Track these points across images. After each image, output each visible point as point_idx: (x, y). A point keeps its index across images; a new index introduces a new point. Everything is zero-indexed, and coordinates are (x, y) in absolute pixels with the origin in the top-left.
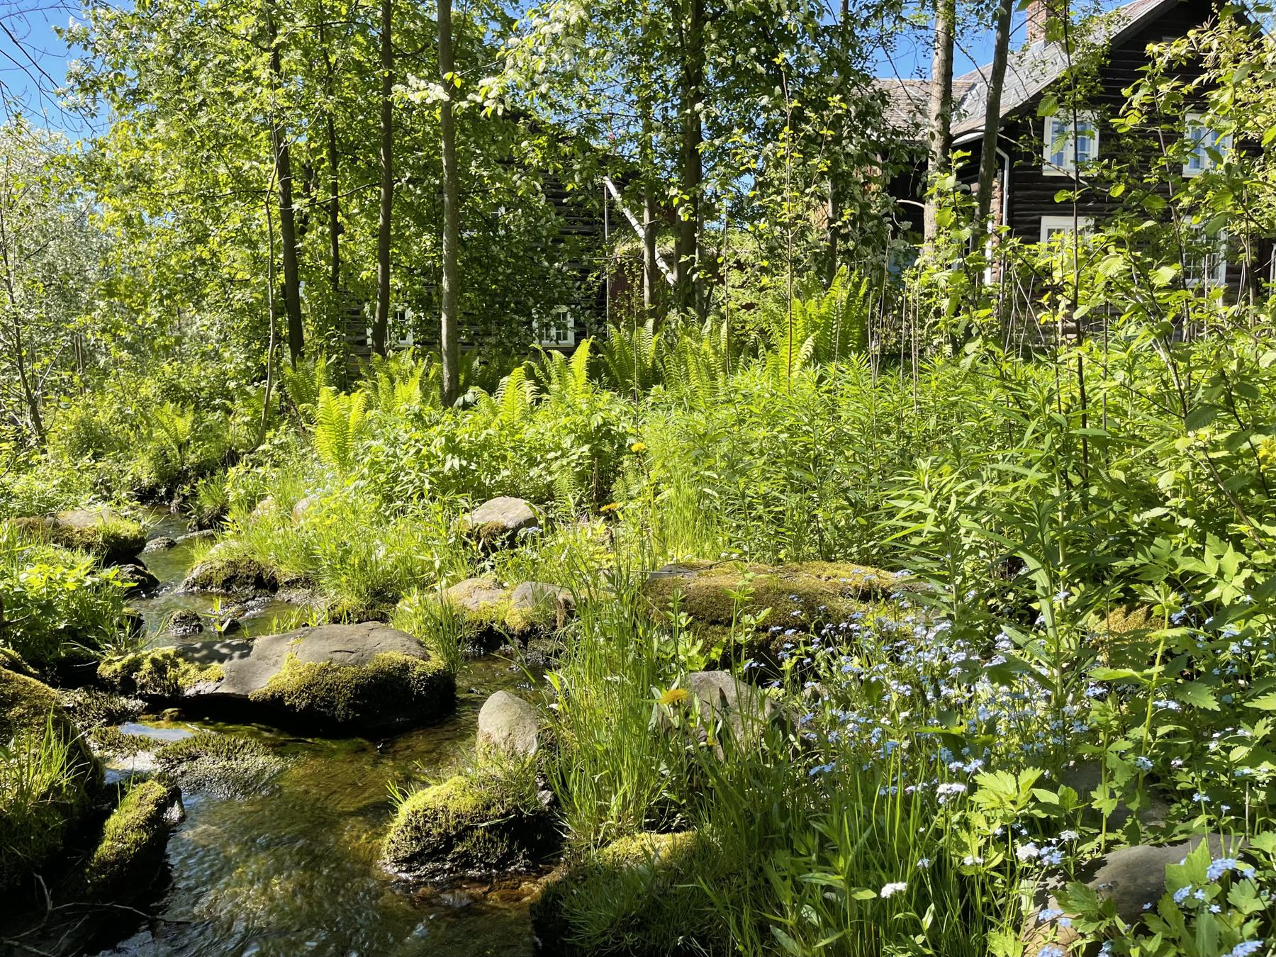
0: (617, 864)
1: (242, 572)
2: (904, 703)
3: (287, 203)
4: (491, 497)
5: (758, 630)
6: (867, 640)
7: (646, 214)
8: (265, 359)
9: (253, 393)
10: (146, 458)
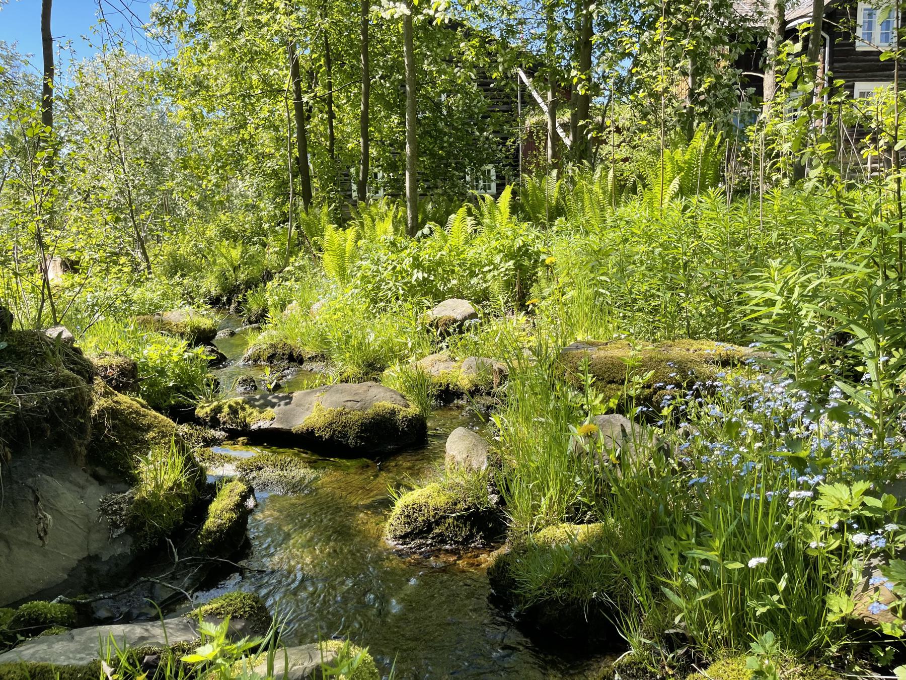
3: (299, 98)
4: (444, 299)
5: (643, 387)
6: (726, 393)
7: (549, 94)
8: (285, 209)
9: (280, 231)
10: (213, 277)
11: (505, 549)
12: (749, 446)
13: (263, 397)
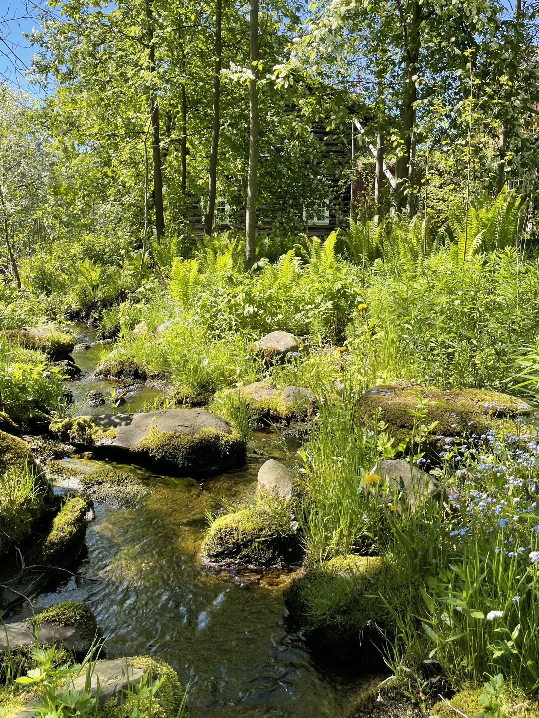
0: (334, 572)
1: (127, 368)
2: (517, 490)
3: (157, 141)
6: (499, 446)
8: (142, 234)
11: (300, 573)
12: (508, 500)
13: (108, 417)
